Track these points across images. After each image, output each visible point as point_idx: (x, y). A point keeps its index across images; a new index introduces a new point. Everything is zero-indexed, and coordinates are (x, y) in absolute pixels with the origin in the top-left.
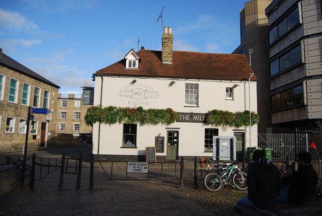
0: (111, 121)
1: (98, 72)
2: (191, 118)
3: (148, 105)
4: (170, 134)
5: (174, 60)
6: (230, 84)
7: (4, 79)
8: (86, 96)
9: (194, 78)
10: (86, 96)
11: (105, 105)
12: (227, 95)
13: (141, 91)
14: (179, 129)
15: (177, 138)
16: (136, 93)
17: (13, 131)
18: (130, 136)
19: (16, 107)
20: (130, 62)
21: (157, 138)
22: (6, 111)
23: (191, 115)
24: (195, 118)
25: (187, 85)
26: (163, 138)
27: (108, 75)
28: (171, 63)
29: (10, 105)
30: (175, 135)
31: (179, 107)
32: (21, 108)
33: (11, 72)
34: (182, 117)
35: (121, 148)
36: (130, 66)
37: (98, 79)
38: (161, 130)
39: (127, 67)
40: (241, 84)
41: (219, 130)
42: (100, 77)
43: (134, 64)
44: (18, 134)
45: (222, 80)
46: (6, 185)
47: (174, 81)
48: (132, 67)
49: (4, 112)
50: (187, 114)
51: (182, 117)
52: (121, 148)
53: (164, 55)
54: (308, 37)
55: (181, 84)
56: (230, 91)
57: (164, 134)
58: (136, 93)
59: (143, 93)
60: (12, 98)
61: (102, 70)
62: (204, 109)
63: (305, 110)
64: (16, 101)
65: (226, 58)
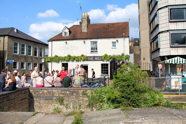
0: (58, 62)
1: (50, 40)
2: (94, 59)
3: (73, 54)
11: (53, 56)
12: (113, 45)
13: (69, 47)
14: (88, 64)
15: (102, 70)
16: (67, 48)
17: (25, 69)
19: (25, 57)
22: (21, 59)
23: (94, 57)
26: (102, 65)
29: (22, 57)
31: (88, 54)
32: (28, 57)
33: (21, 41)
34: (89, 59)
36: (65, 35)
42: (51, 42)
43: (67, 35)
44: (27, 70)
49: (20, 60)
50: (91, 57)
51: (99, 59)
54: (161, 8)
55: (88, 42)
58: (67, 48)
59: (70, 48)
60: (23, 53)
61: (52, 38)
63: (158, 53)
64: (25, 54)
65: (117, 25)
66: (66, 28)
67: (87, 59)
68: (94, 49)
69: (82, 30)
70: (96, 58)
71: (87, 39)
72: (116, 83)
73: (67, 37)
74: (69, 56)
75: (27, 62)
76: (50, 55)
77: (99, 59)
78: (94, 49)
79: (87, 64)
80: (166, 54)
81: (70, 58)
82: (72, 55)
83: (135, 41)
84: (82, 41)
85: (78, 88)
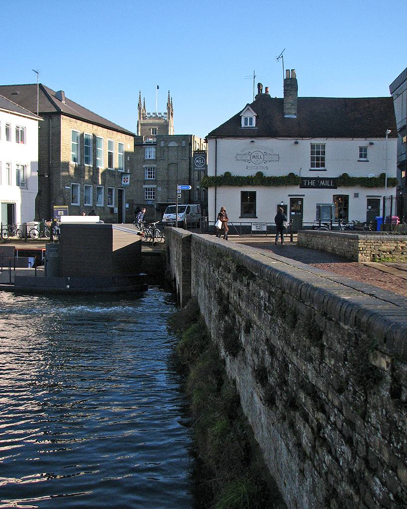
2: (318, 183)
4: (294, 201)
5: (298, 112)
6: (362, 142)
7: (100, 183)
8: (197, 161)
9: (321, 137)
10: (197, 161)
11: (221, 173)
13: (260, 154)
14: (304, 195)
16: (254, 157)
18: (249, 205)
20: (246, 119)
21: (279, 206)
23: (318, 180)
24: (322, 183)
25: (312, 146)
27: (222, 137)
28: (55, 207)
30: (300, 203)
34: (307, 182)
35: (240, 217)
36: (246, 124)
37: (212, 142)
38: (283, 195)
39: (243, 125)
40: (376, 141)
41: (350, 196)
43: (251, 123)
45: (354, 138)
46: (231, 508)
47: (297, 141)
48: (248, 126)
51: (307, 182)
52: (240, 217)
53: (287, 106)
55: (306, 144)
56: (363, 153)
57: (287, 202)
58: (254, 157)
59: (262, 157)
62: (332, 171)
65: (367, 105)
66: (248, 107)
67: (304, 183)
68: (318, 160)
69: (284, 114)
70: (322, 183)
71: (303, 136)
72: (228, 390)
73: (250, 129)
74: (260, 174)
75: (95, 185)
76: (211, 173)
77: (330, 184)
78: (318, 160)
79: (303, 194)
80: (33, 210)
81: (261, 180)
82: (268, 173)
83: (364, 355)
84: (290, 142)
85: (207, 276)
